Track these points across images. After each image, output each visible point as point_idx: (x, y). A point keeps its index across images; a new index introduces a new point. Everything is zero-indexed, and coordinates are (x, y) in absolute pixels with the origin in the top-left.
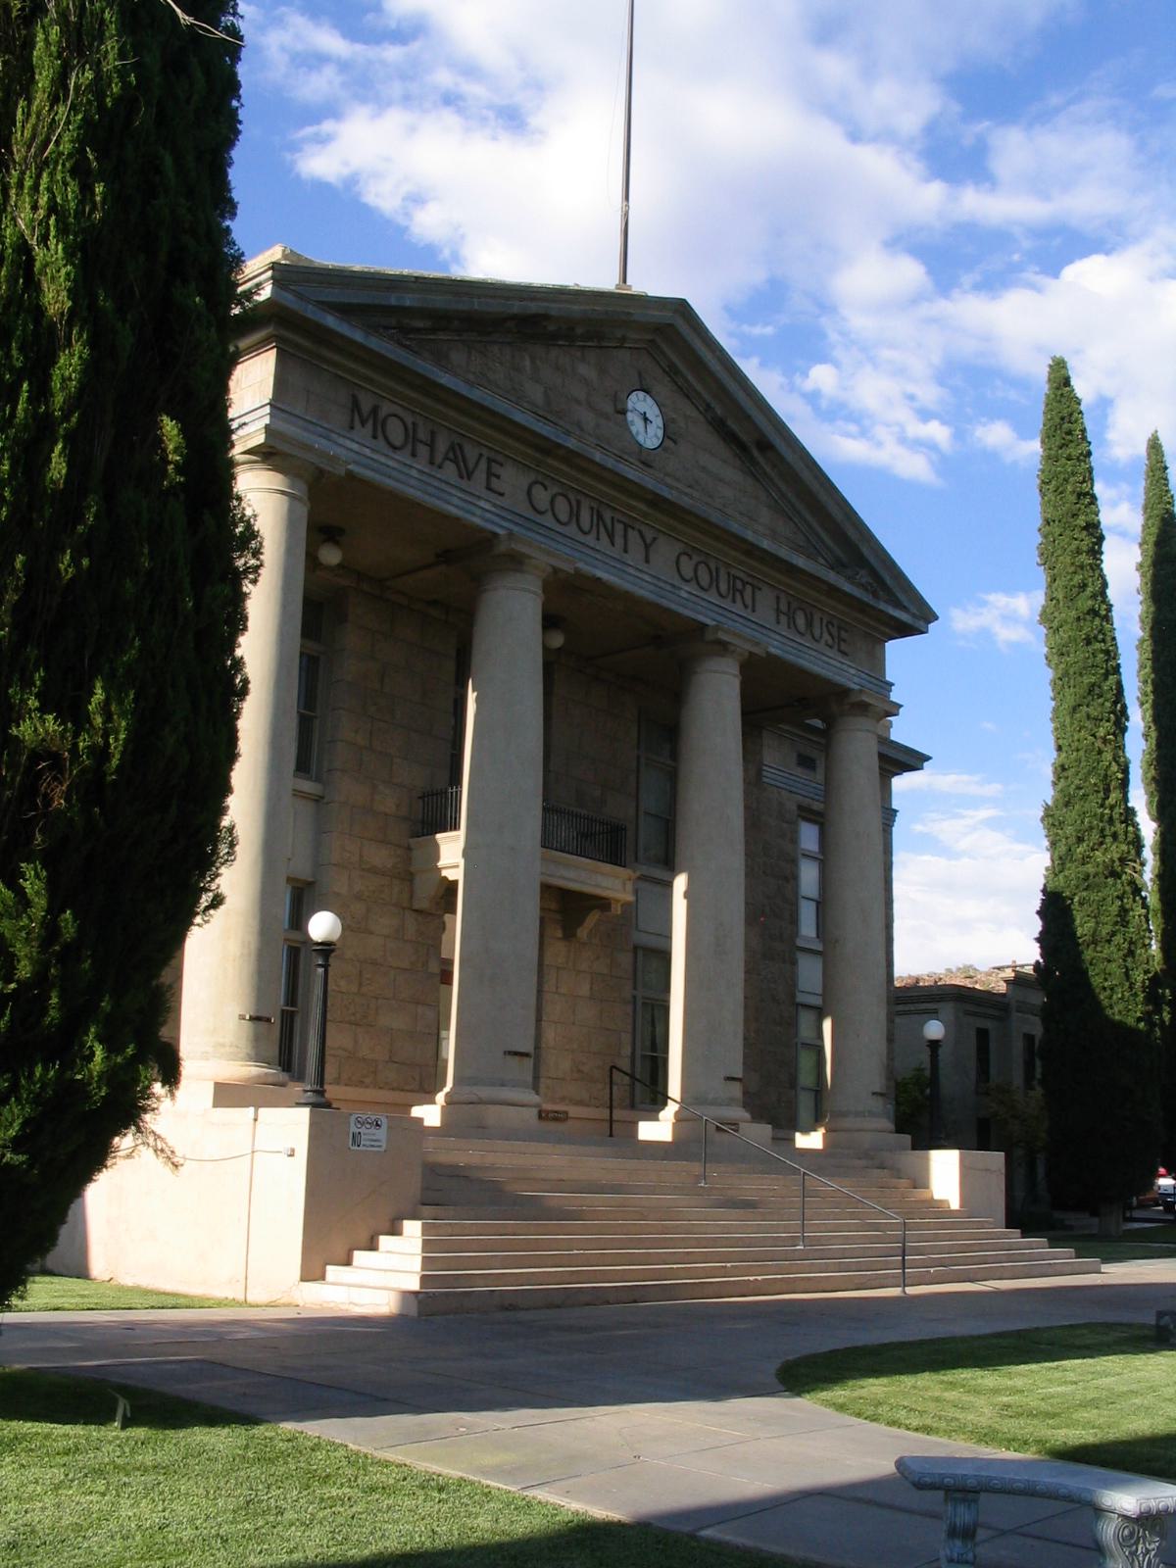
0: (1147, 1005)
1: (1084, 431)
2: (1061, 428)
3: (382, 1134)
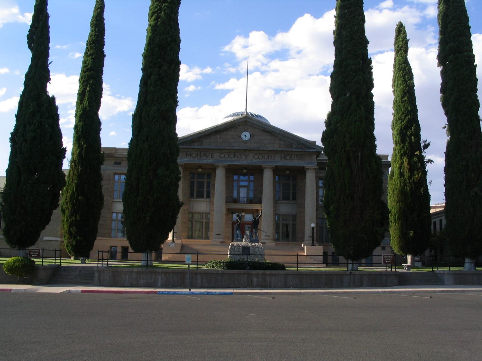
0: (69, 239)
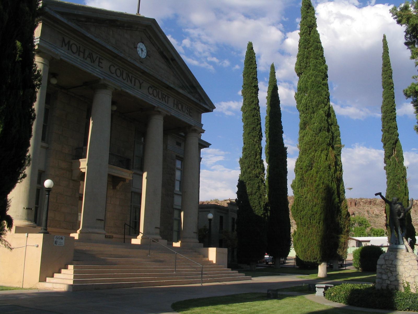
1: (255, 62)
2: (250, 60)
3: (63, 241)
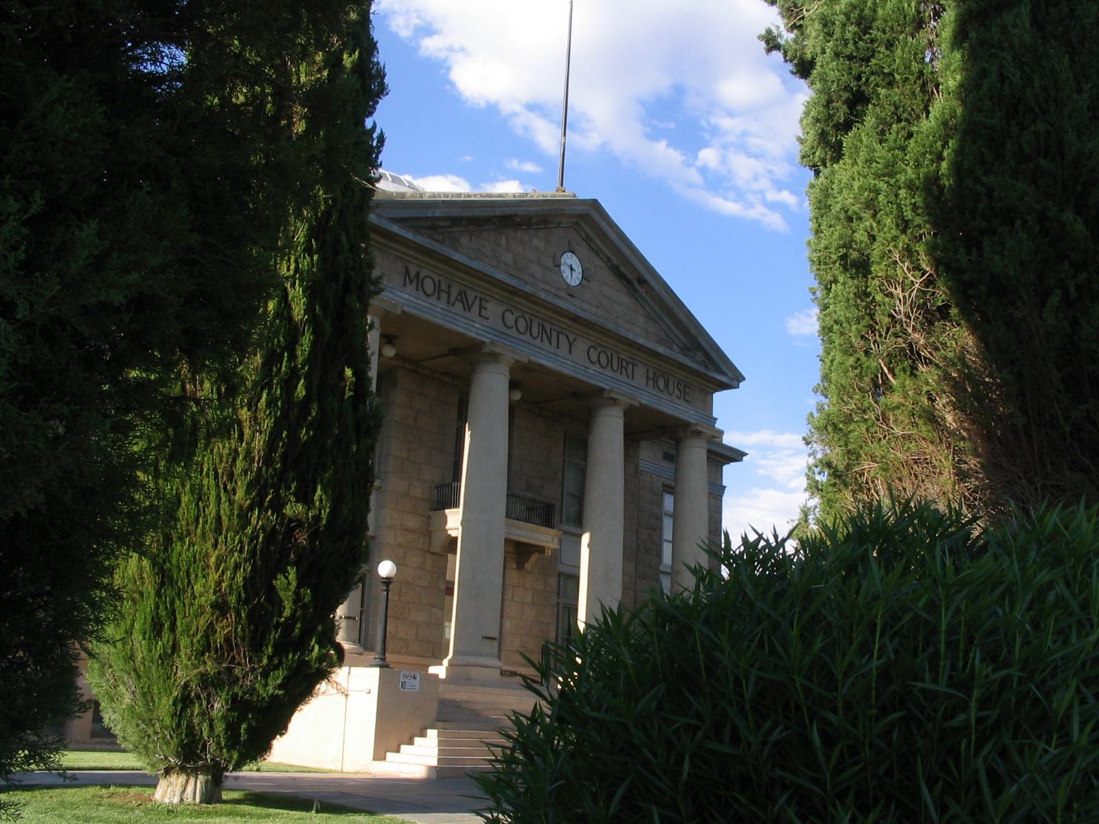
3: (417, 682)
